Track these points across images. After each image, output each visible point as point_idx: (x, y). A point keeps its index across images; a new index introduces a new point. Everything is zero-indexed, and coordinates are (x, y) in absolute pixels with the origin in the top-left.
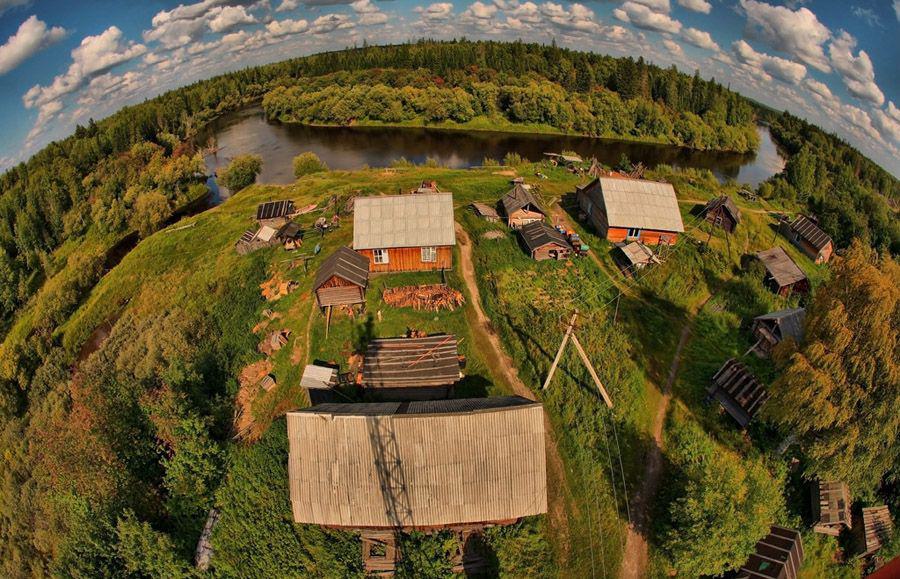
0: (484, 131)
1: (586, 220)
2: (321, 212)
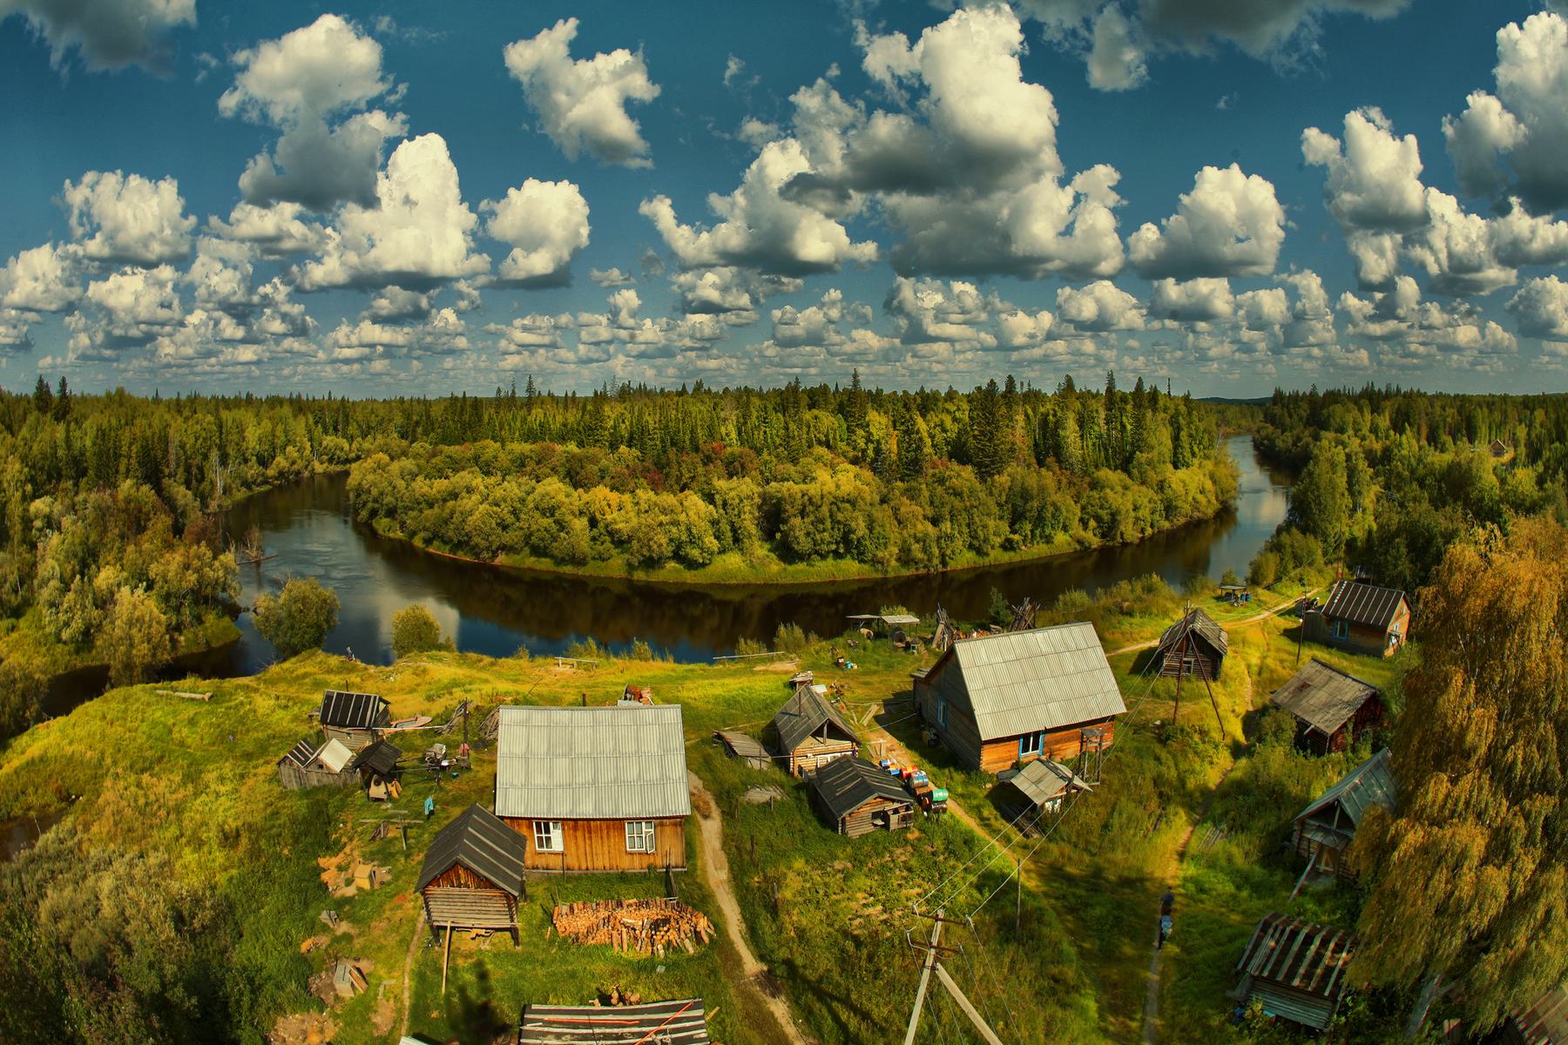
0: (737, 586)
1: (937, 742)
2: (438, 733)
